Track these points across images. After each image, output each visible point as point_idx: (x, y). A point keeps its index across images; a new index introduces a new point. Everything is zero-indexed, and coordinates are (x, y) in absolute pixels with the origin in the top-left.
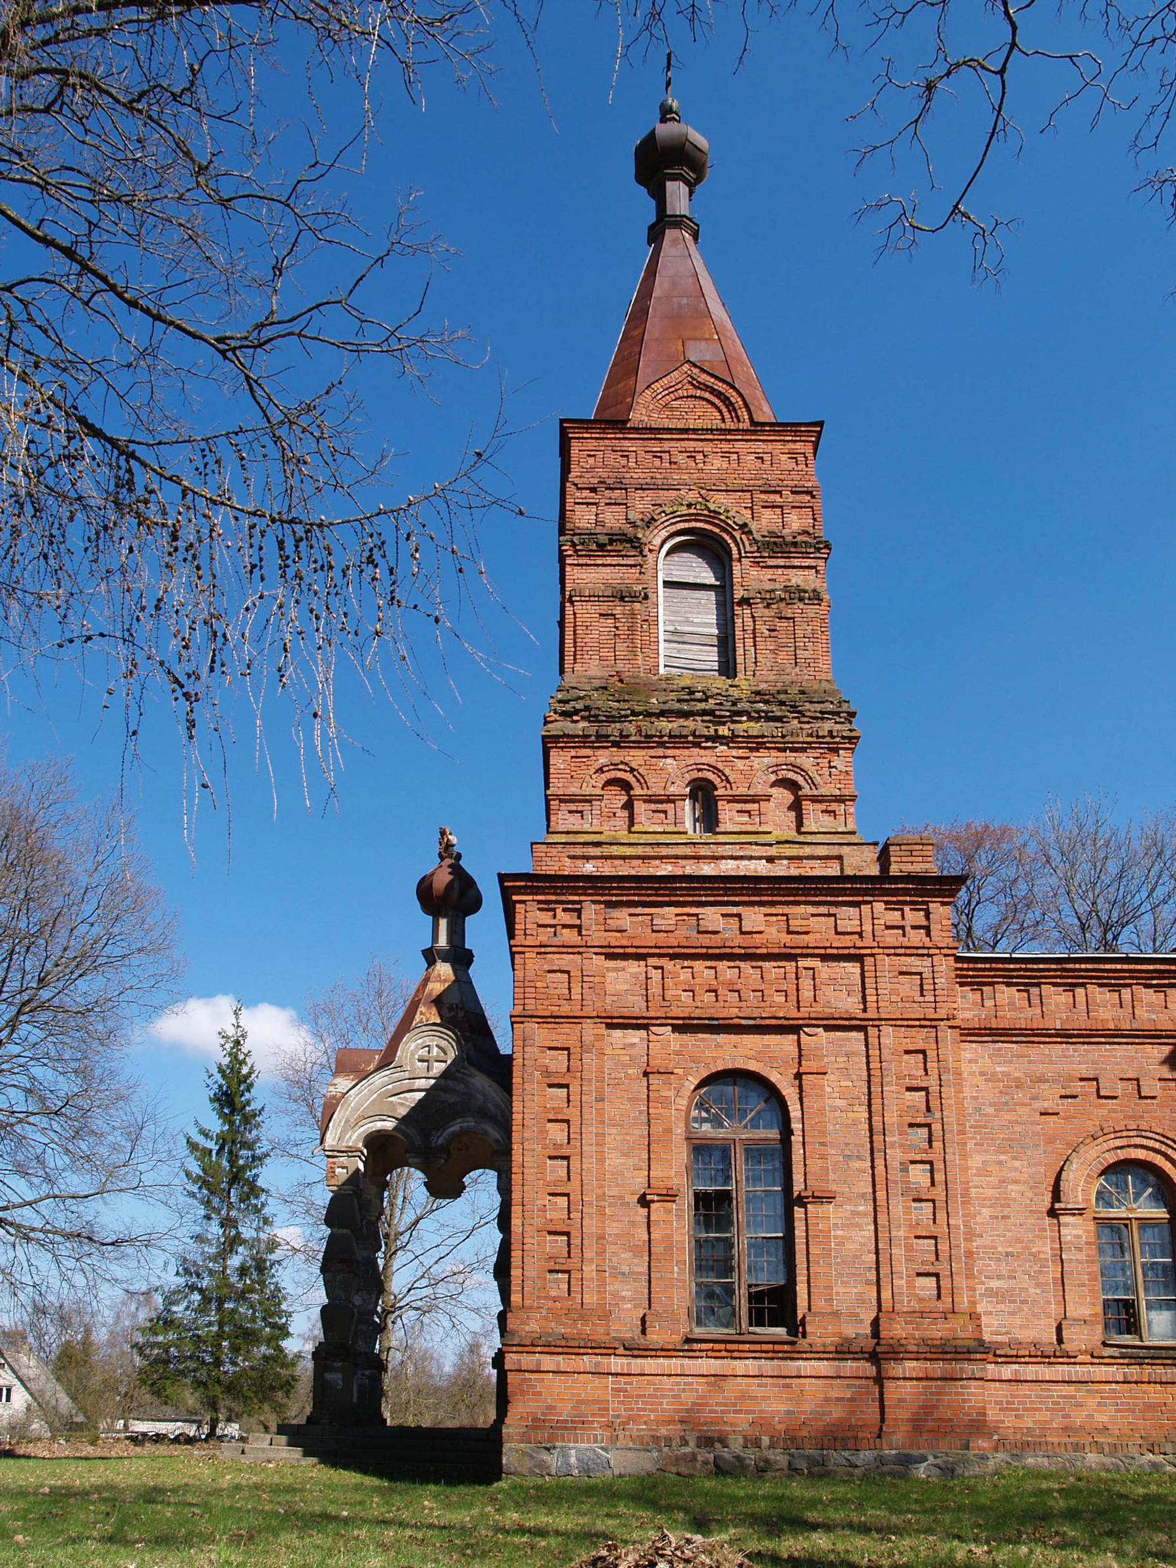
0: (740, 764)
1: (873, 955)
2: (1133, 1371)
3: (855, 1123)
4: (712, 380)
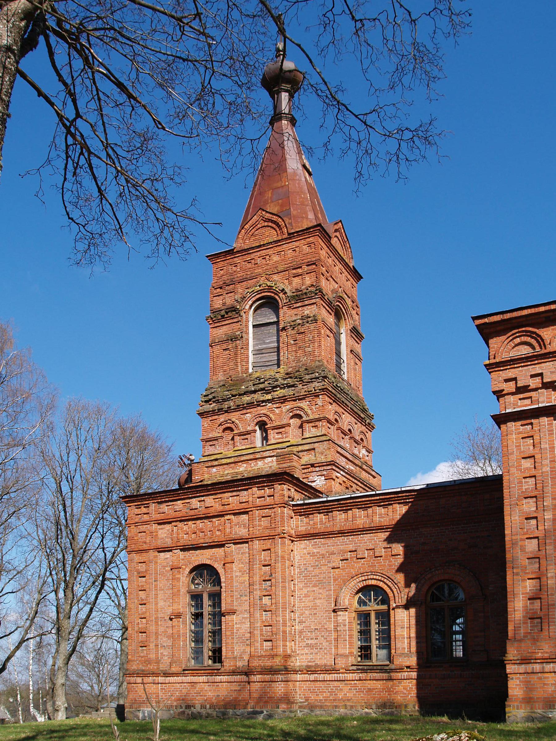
0: (277, 411)
1: (251, 511)
2: (363, 676)
3: (245, 581)
4: (271, 216)
